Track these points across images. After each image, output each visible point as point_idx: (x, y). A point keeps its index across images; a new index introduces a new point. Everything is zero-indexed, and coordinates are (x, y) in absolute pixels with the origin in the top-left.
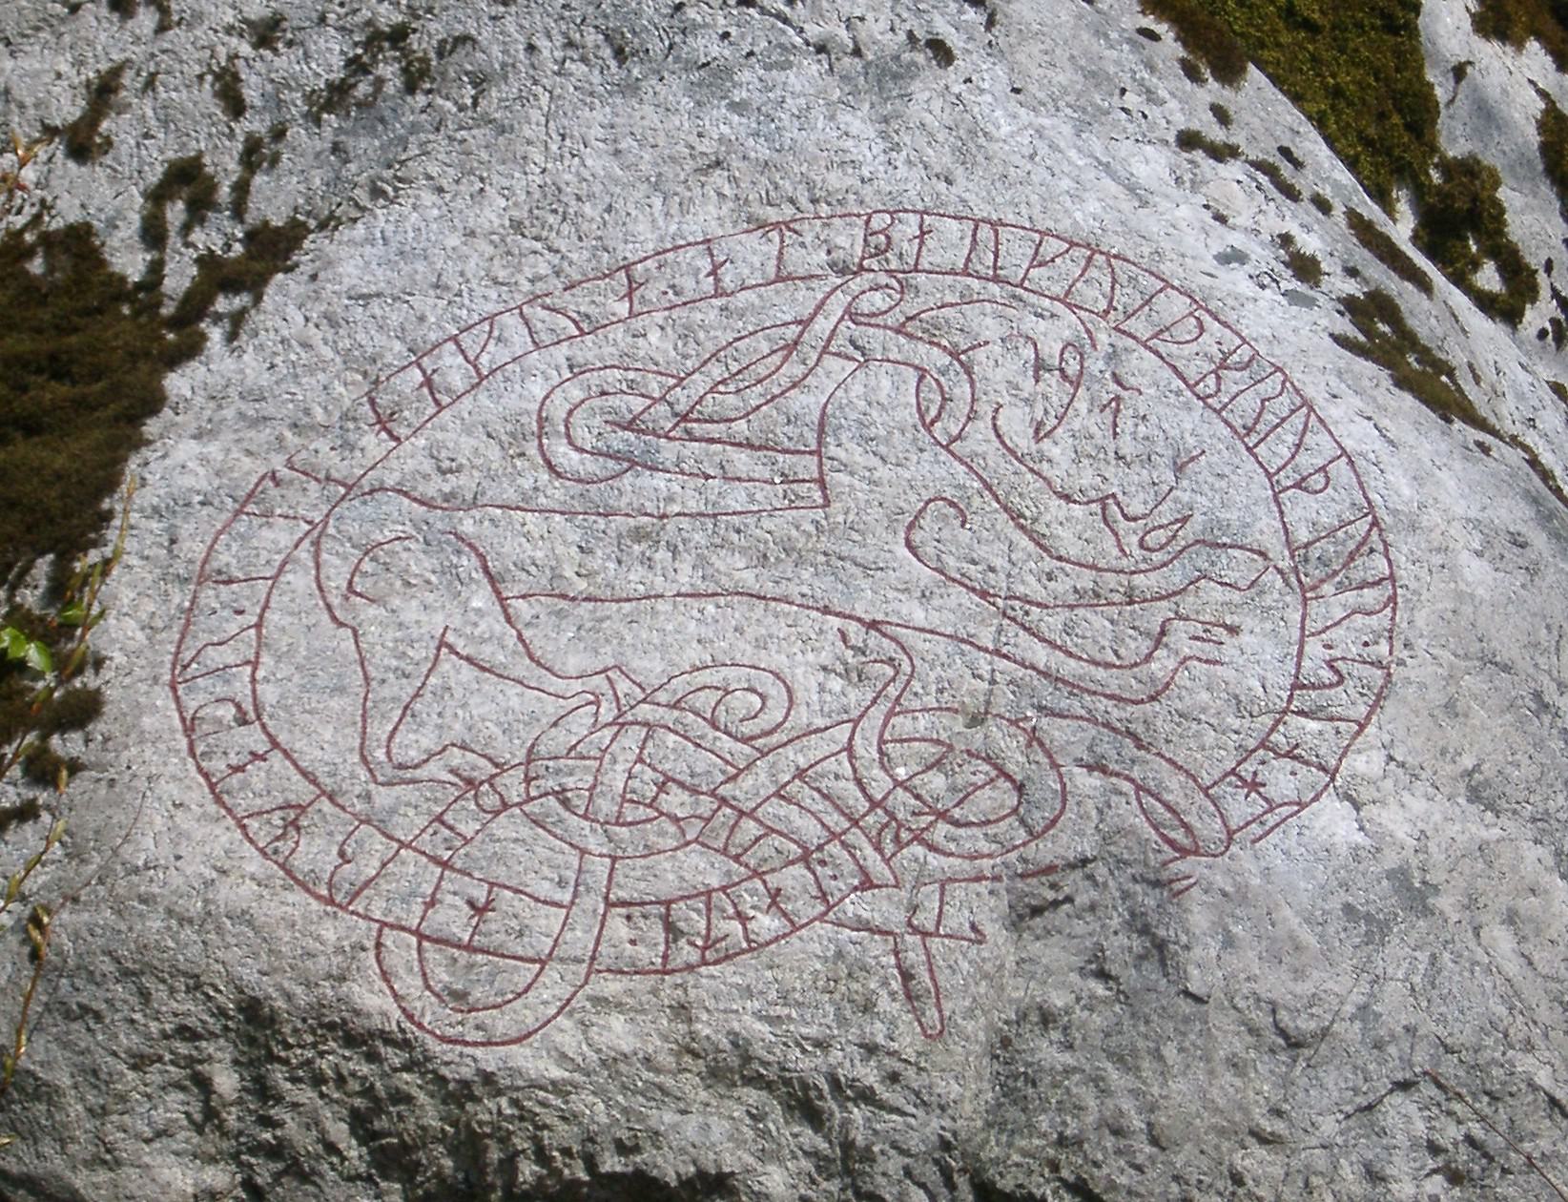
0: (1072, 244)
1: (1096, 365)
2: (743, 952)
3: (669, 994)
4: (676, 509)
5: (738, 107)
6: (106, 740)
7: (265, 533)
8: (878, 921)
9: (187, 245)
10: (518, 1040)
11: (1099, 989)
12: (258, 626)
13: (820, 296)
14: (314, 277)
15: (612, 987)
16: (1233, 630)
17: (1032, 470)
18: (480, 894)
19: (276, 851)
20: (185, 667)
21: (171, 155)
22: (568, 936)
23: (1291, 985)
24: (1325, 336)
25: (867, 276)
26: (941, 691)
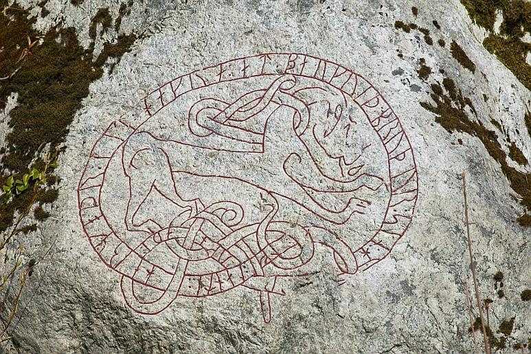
0: (347, 70)
1: (345, 113)
2: (219, 293)
3: (198, 304)
4: (223, 148)
5: (259, 13)
6: (57, 207)
7: (110, 142)
8: (257, 287)
9: (102, 38)
10: (155, 314)
11: (316, 310)
12: (104, 173)
13: (272, 81)
14: (135, 55)
15: (182, 300)
16: (369, 203)
17: (321, 146)
18: (151, 269)
19: (98, 249)
20: (83, 185)
21: (100, 7)
22: (172, 283)
23: (369, 314)
24: (418, 103)
25: (287, 76)
26: (285, 216)
